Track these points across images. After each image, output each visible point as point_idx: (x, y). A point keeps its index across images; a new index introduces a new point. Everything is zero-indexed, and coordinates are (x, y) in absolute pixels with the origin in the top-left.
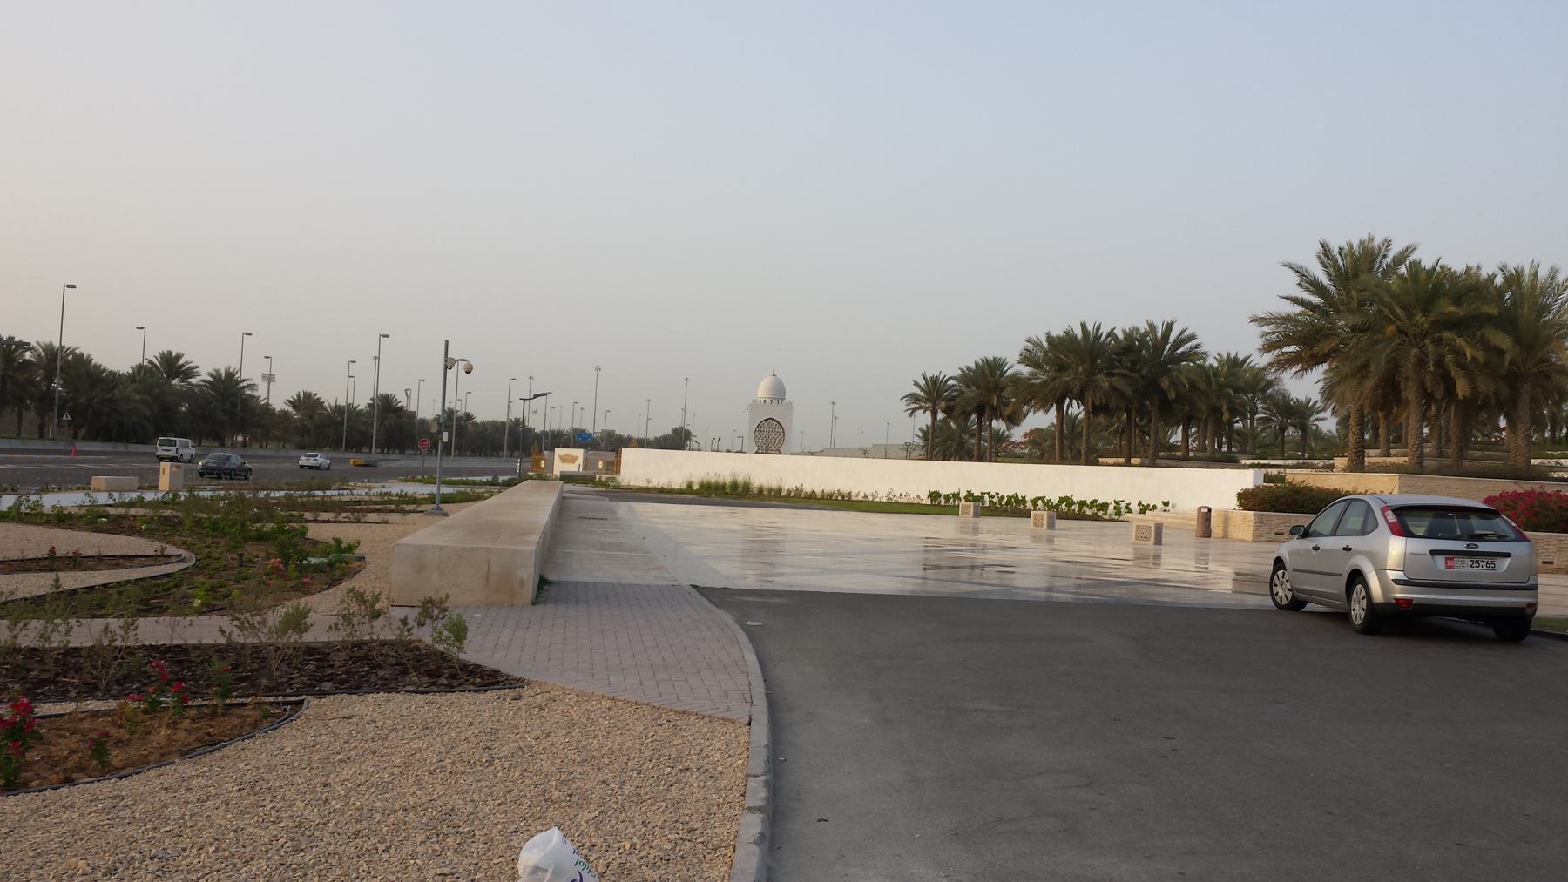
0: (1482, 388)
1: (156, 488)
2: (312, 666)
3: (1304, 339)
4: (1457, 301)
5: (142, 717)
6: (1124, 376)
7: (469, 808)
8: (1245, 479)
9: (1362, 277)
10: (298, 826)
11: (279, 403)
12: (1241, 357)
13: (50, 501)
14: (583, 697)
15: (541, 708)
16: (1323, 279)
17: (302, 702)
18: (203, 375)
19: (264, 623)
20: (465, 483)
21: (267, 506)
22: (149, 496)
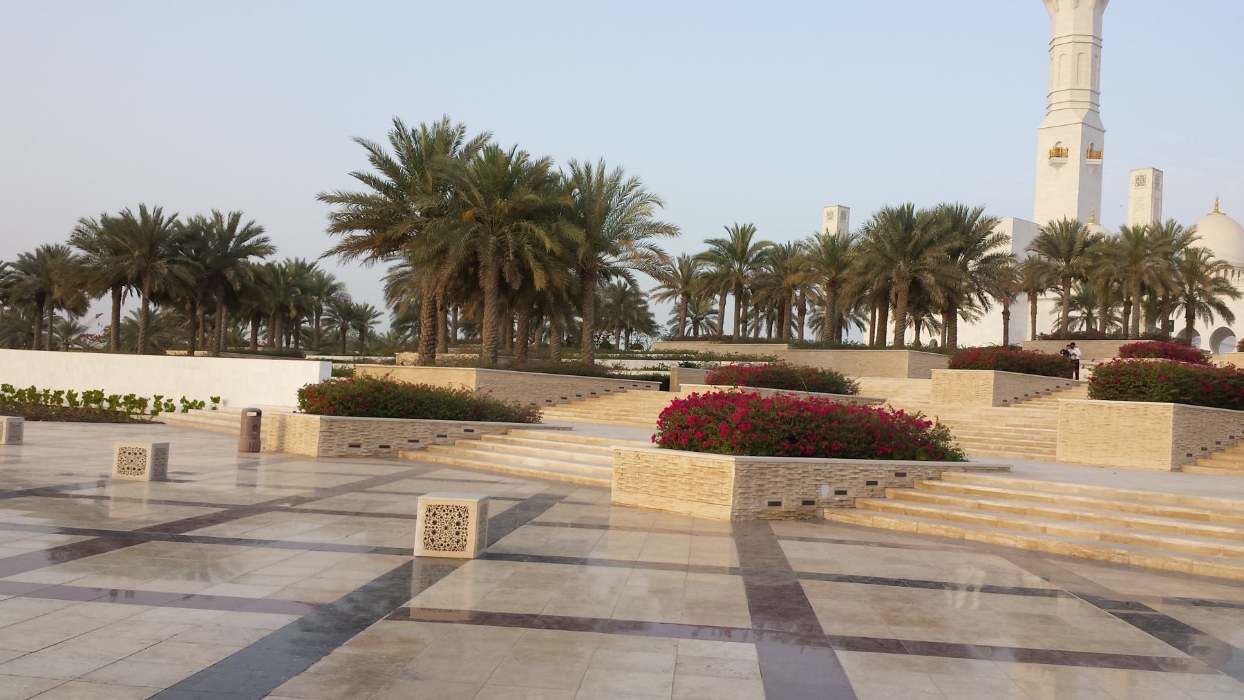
4: (536, 188)
6: (186, 264)
8: (311, 371)
9: (438, 158)
12: (308, 263)
16: (396, 160)
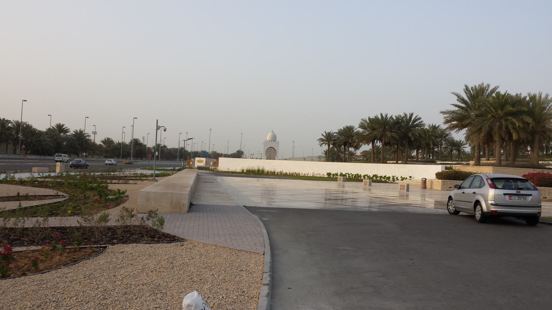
0: (522, 136)
1: (55, 171)
2: (110, 234)
3: (459, 119)
4: (513, 106)
5: (50, 252)
6: (396, 132)
7: (165, 284)
8: (438, 168)
9: (480, 97)
10: (105, 290)
11: (98, 142)
12: (437, 126)
13: (18, 176)
14: (205, 245)
15: (191, 249)
16: (466, 98)
17: (106, 247)
18: (72, 132)
19: (93, 219)
20: (164, 170)
21: (94, 178)
22: (53, 174)
